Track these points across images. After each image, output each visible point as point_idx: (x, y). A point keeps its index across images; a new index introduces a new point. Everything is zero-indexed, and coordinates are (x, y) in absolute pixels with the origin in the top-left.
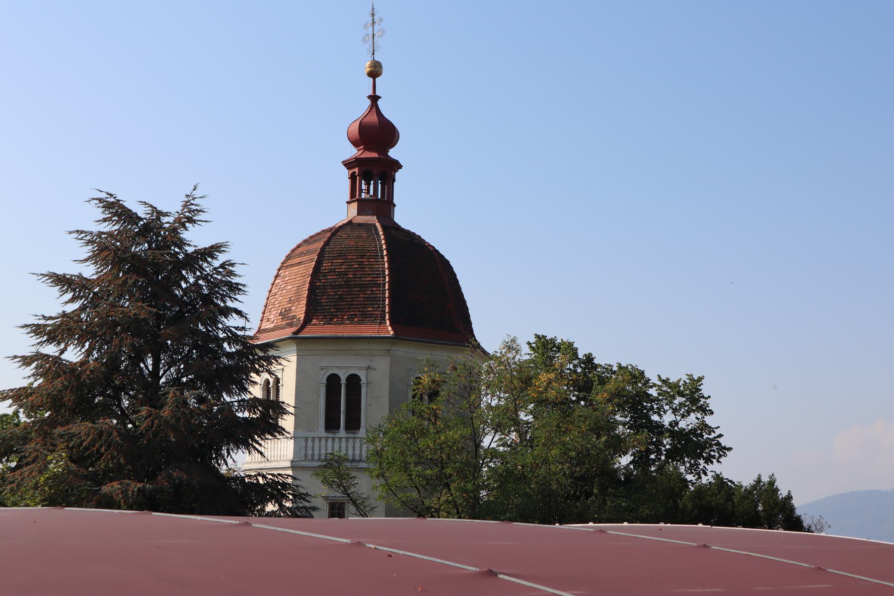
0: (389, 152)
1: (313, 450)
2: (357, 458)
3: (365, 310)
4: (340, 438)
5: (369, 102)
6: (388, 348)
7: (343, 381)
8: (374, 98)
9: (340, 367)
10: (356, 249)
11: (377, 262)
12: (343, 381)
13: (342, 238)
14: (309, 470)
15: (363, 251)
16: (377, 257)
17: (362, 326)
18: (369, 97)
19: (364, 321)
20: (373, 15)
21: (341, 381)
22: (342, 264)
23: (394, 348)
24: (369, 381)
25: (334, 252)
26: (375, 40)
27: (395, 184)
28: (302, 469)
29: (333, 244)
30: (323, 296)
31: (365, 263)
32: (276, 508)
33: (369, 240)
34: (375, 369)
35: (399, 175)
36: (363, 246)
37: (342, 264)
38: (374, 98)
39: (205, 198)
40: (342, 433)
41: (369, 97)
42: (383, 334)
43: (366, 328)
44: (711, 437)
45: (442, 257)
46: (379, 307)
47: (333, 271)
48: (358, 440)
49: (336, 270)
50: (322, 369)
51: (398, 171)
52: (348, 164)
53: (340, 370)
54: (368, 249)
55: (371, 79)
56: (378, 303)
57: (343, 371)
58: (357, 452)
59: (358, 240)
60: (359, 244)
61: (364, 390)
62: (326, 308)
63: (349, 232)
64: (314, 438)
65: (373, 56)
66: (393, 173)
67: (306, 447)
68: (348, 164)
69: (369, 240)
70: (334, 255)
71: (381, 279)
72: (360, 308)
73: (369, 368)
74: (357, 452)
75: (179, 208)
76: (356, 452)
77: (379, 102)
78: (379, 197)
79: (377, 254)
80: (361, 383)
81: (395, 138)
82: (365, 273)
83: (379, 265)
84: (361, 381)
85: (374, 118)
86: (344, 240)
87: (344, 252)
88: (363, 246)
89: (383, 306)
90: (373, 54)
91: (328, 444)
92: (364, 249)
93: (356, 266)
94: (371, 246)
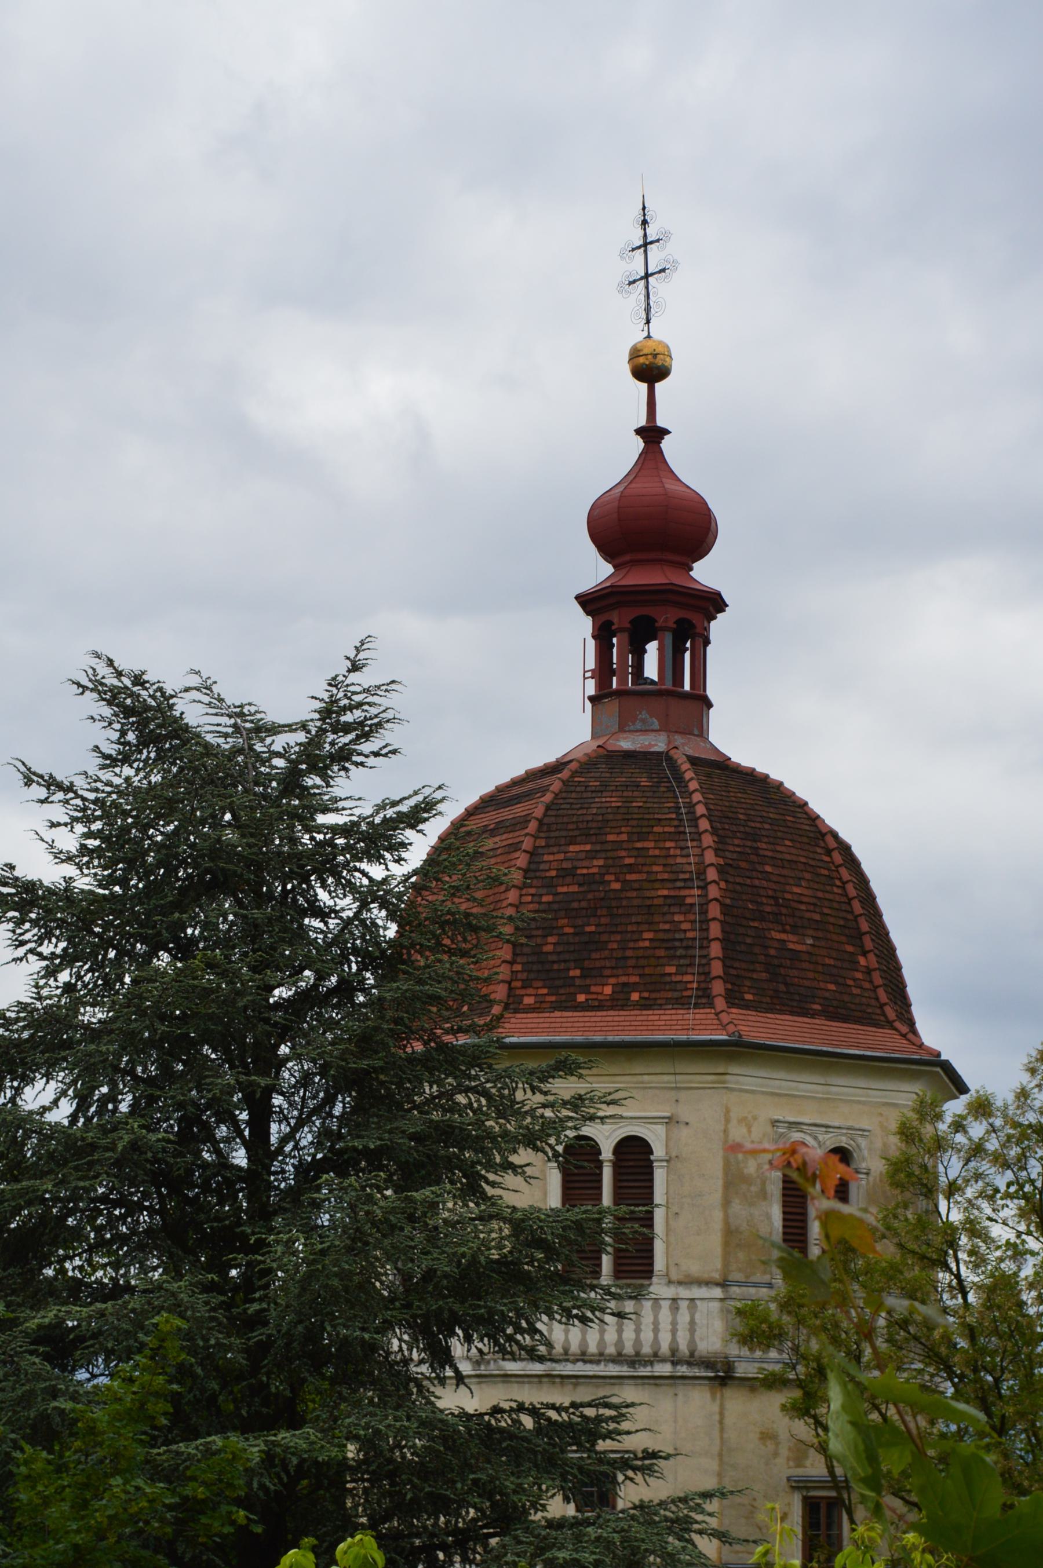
0: (691, 569)
2: (646, 1350)
3: (659, 970)
5: (638, 444)
7: (607, 1153)
10: (627, 817)
11: (682, 849)
12: (607, 1153)
13: (589, 789)
15: (646, 823)
16: (682, 837)
17: (651, 1012)
18: (639, 432)
19: (655, 999)
20: (645, 223)
21: (600, 1153)
22: (591, 855)
23: (734, 1069)
24: (674, 1154)
25: (571, 827)
26: (650, 288)
27: (709, 649)
28: (504, 1382)
29: (568, 806)
30: (545, 936)
31: (651, 853)
33: (658, 795)
34: (687, 1124)
35: (717, 628)
36: (641, 811)
37: (591, 855)
41: (639, 432)
42: (709, 1032)
43: (663, 1017)
44: (99, 1305)
46: (691, 965)
47: (570, 873)
49: (579, 871)
51: (715, 618)
52: (588, 602)
54: (656, 816)
55: (644, 386)
56: (690, 952)
58: (647, 1336)
59: (630, 794)
60: (634, 804)
61: (660, 1176)
62: (556, 967)
63: (603, 775)
64: (692, 1300)
65: (646, 328)
66: (706, 624)
68: (588, 602)
69: (658, 795)
70: (571, 833)
71: (696, 892)
72: (643, 967)
73: (670, 1121)
74: (647, 1336)
75: (306, 710)
76: (642, 1335)
77: (666, 444)
78: (687, 687)
79: (682, 829)
80: (652, 1158)
81: (711, 535)
82: (653, 877)
83: (689, 856)
84: (652, 1153)
85: (648, 486)
86: (594, 795)
87: (594, 825)
88: (641, 811)
89: (704, 961)
90: (648, 322)
92: (647, 816)
93: (627, 861)
94: (667, 810)
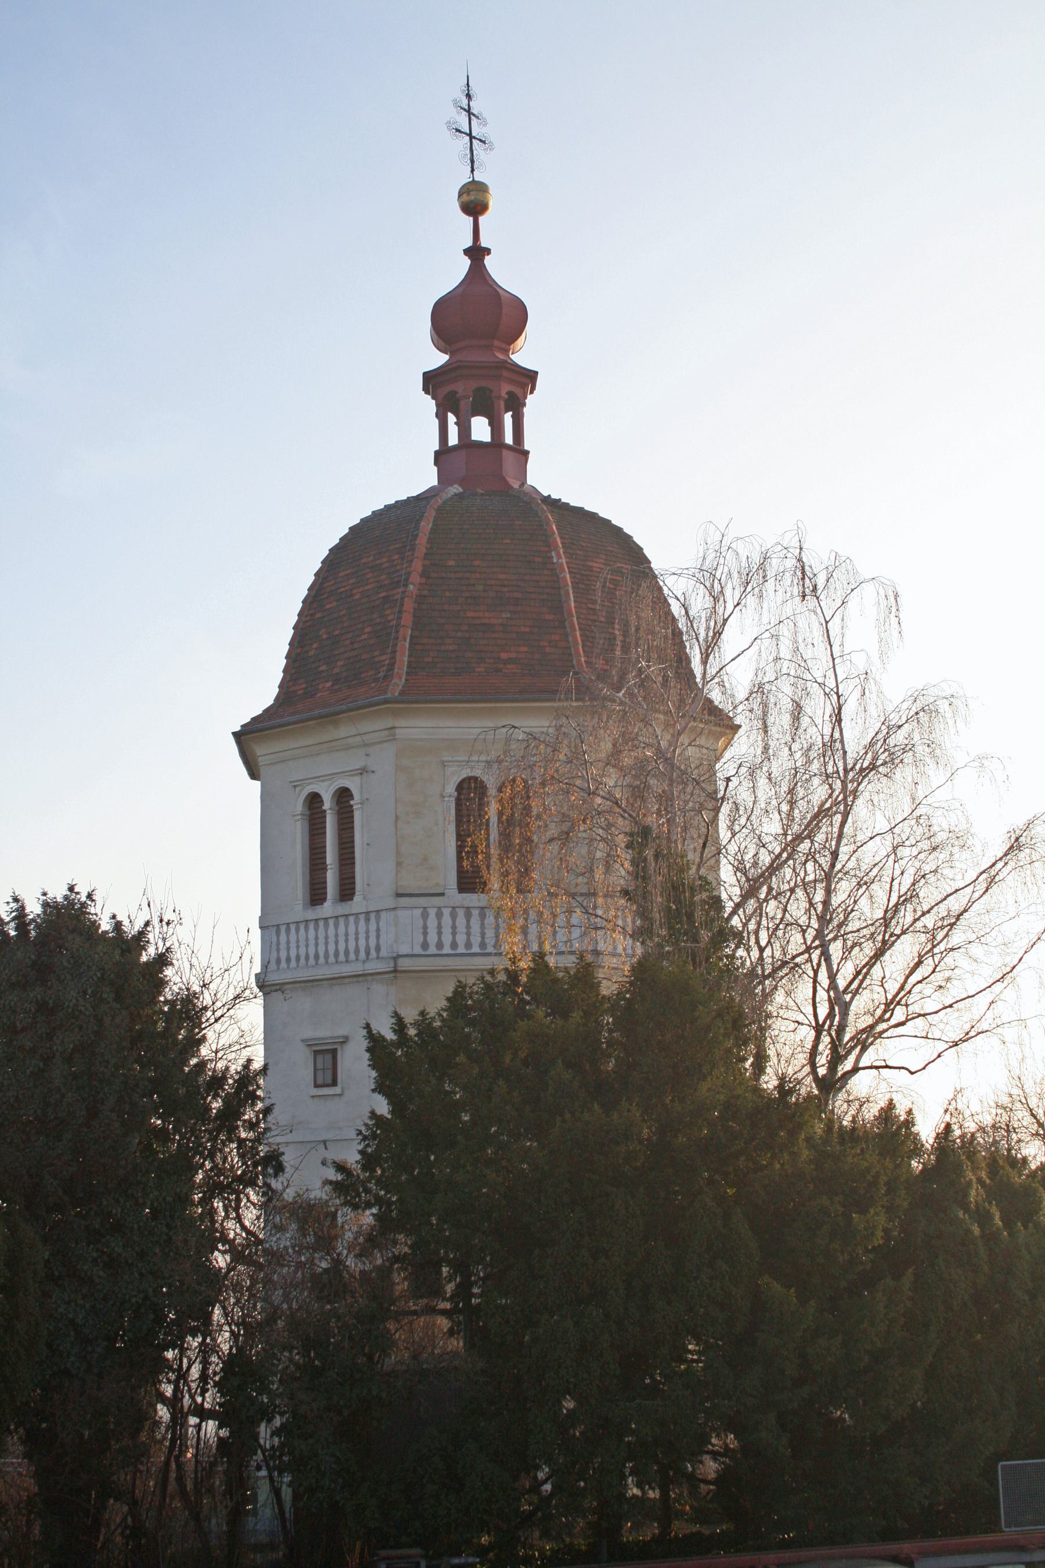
1: (337, 943)
4: (326, 919)
5: (466, 263)
6: (390, 725)
8: (477, 253)
9: (319, 777)
14: (350, 983)
23: (401, 722)
32: (850, 995)
34: (373, 772)
38: (477, 253)
39: (899, 589)
40: (328, 908)
41: (467, 252)
45: (388, 508)
48: (352, 919)
50: (295, 787)
53: (321, 783)
57: (326, 783)
67: (378, 937)
77: (488, 261)
91: (319, 932)
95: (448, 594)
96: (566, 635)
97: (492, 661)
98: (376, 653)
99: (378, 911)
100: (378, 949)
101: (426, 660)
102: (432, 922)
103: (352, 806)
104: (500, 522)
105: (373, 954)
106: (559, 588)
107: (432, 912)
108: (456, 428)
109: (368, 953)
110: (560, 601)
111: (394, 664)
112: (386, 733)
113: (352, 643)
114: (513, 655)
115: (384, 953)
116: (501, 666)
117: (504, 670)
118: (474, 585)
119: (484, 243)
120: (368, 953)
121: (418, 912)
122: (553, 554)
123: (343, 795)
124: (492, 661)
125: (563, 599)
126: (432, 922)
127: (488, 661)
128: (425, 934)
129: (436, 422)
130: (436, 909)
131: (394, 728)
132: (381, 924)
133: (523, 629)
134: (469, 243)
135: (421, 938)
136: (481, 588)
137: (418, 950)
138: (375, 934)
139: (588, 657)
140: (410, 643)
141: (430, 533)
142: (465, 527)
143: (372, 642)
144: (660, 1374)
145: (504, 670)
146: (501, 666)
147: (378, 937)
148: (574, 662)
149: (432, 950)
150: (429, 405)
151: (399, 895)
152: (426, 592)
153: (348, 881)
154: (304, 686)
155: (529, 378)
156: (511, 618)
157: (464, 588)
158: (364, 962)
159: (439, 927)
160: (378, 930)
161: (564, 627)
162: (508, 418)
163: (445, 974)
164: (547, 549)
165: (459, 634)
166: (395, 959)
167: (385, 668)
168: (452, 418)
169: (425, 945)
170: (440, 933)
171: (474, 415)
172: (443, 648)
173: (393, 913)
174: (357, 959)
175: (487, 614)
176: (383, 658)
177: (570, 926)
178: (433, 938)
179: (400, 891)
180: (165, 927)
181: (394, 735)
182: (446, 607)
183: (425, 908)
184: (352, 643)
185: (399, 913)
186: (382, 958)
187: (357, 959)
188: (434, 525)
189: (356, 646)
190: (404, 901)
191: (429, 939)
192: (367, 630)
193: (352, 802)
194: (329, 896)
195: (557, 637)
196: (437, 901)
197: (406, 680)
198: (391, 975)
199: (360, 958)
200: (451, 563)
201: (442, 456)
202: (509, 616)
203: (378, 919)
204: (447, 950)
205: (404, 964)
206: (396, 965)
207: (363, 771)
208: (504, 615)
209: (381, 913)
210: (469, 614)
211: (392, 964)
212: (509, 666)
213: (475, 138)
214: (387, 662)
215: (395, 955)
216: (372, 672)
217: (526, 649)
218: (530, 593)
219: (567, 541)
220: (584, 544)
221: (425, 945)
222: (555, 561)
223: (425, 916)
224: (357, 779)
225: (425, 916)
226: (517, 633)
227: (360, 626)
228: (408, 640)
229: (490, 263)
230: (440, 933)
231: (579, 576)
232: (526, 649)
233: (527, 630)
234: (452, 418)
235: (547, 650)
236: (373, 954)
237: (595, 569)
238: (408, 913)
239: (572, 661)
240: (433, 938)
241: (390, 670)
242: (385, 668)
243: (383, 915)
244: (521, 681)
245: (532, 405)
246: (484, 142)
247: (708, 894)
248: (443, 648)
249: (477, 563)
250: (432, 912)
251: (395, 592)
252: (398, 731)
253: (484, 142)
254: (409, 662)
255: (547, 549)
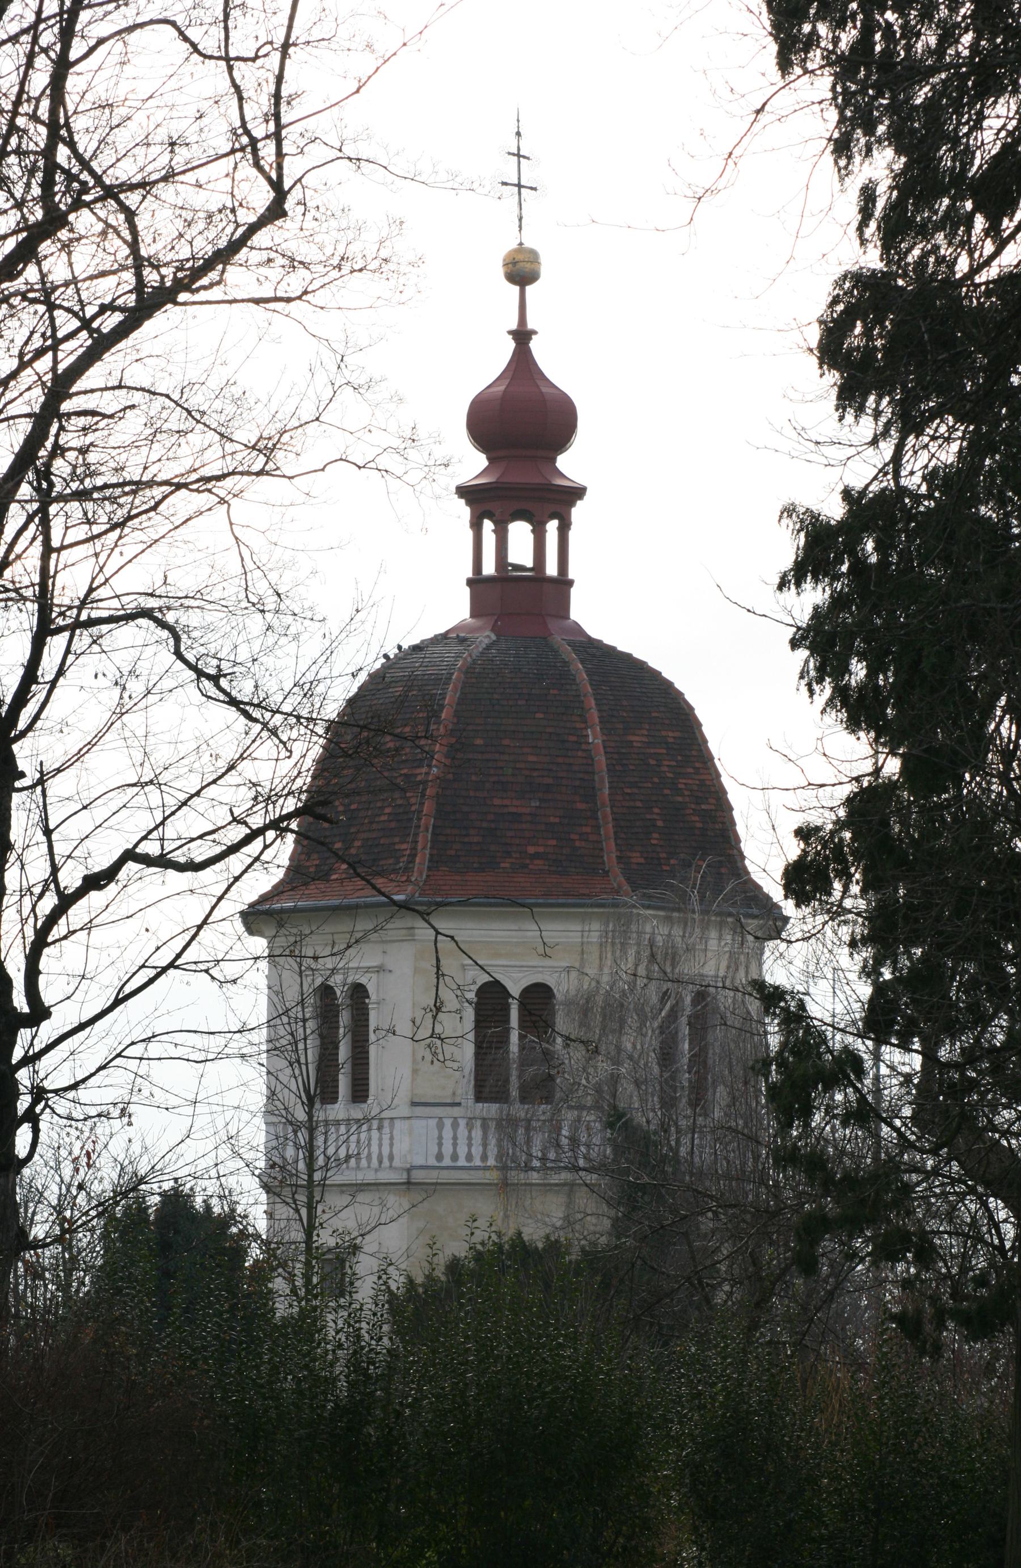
5: (510, 345)
6: (410, 925)
8: (522, 336)
38: (522, 336)
67: (391, 1145)
77: (533, 345)
95: (474, 778)
96: (598, 827)
97: (518, 855)
98: (397, 840)
99: (392, 1119)
100: (391, 1158)
101: (449, 852)
102: (448, 1133)
103: (367, 1005)
104: (533, 691)
105: (386, 1163)
106: (593, 773)
107: (448, 1123)
108: (493, 536)
109: (380, 1162)
110: (594, 788)
111: (415, 855)
112: (404, 932)
113: (371, 823)
114: (541, 850)
115: (397, 1163)
116: (528, 861)
117: (530, 867)
118: (502, 768)
119: (530, 326)
120: (380, 1162)
121: (433, 1123)
122: (589, 731)
123: (359, 992)
124: (518, 855)
125: (597, 786)
126: (448, 1133)
127: (514, 855)
128: (440, 1145)
129: (469, 534)
130: (451, 1120)
131: (413, 928)
132: (395, 1132)
133: (552, 820)
134: (514, 326)
135: (436, 1150)
136: (510, 771)
137: (432, 1162)
138: (388, 1142)
139: (621, 851)
140: (433, 834)
141: (458, 704)
142: (496, 696)
143: (393, 825)
144: (891, 320)
145: (530, 867)
146: (528, 861)
147: (391, 1145)
148: (605, 858)
149: (447, 1162)
150: (463, 511)
151: (414, 1104)
152: (450, 776)
153: (361, 1082)
154: (317, 862)
155: (577, 493)
156: (540, 807)
157: (492, 772)
158: (376, 1170)
159: (455, 1138)
160: (392, 1138)
161: (597, 819)
162: (552, 527)
163: (458, 1187)
164: (583, 726)
165: (485, 825)
166: (409, 1171)
167: (405, 858)
168: (488, 526)
169: (439, 1157)
170: (455, 1145)
171: (513, 520)
172: (466, 840)
173: (407, 1122)
174: (369, 1167)
175: (515, 802)
176: (404, 846)
177: (588, 1146)
178: (447, 1149)
179: (416, 1100)
180: (120, 112)
181: (413, 935)
182: (472, 794)
183: (440, 1118)
184: (371, 823)
185: (413, 1121)
186: (396, 1168)
187: (369, 1167)
188: (462, 693)
189: (374, 826)
190: (419, 1111)
191: (443, 1150)
192: (387, 810)
193: (367, 1001)
194: (340, 1099)
195: (588, 830)
196: (456, 1111)
197: (428, 876)
198: (404, 1187)
199: (372, 1165)
200: (479, 742)
201: (477, 583)
202: (538, 804)
203: (392, 1127)
204: (462, 1162)
205: (418, 1176)
206: (409, 1178)
207: (380, 969)
208: (533, 804)
209: (396, 1121)
210: (497, 802)
211: (405, 1175)
212: (536, 862)
213: (524, 187)
214: (408, 852)
215: (408, 1166)
216: (391, 861)
217: (554, 842)
218: (562, 778)
219: (605, 714)
220: (625, 714)
221: (439, 1157)
222: (591, 741)
223: (440, 1126)
224: (374, 976)
225: (440, 1126)
226: (546, 824)
227: (379, 804)
228: (430, 830)
229: (535, 345)
230: (455, 1145)
231: (616, 756)
232: (554, 842)
233: (557, 820)
234: (488, 526)
235: (577, 844)
236: (386, 1163)
237: (635, 744)
238: (423, 1122)
239: (602, 857)
240: (447, 1149)
241: (410, 862)
242: (405, 858)
243: (397, 1123)
244: (548, 880)
245: (578, 512)
246: (535, 189)
247: (814, 684)
248: (466, 840)
249: (506, 742)
250: (448, 1123)
251: (418, 771)
252: (416, 931)
253: (535, 189)
254: (431, 855)
255: (583, 726)
